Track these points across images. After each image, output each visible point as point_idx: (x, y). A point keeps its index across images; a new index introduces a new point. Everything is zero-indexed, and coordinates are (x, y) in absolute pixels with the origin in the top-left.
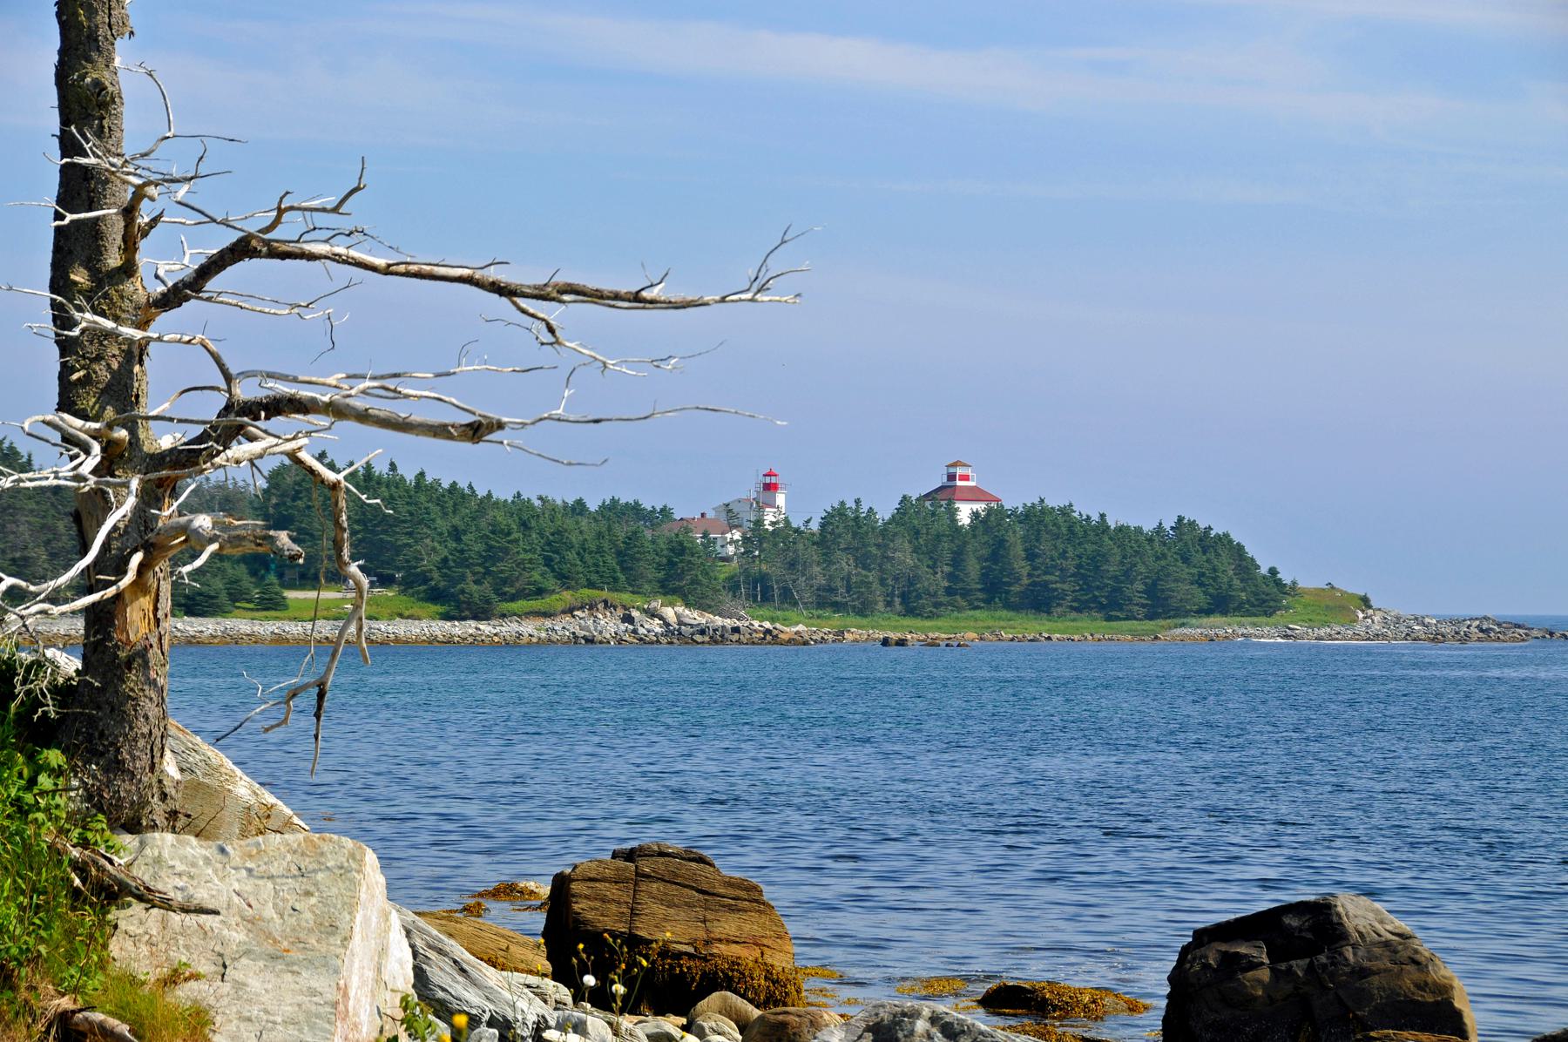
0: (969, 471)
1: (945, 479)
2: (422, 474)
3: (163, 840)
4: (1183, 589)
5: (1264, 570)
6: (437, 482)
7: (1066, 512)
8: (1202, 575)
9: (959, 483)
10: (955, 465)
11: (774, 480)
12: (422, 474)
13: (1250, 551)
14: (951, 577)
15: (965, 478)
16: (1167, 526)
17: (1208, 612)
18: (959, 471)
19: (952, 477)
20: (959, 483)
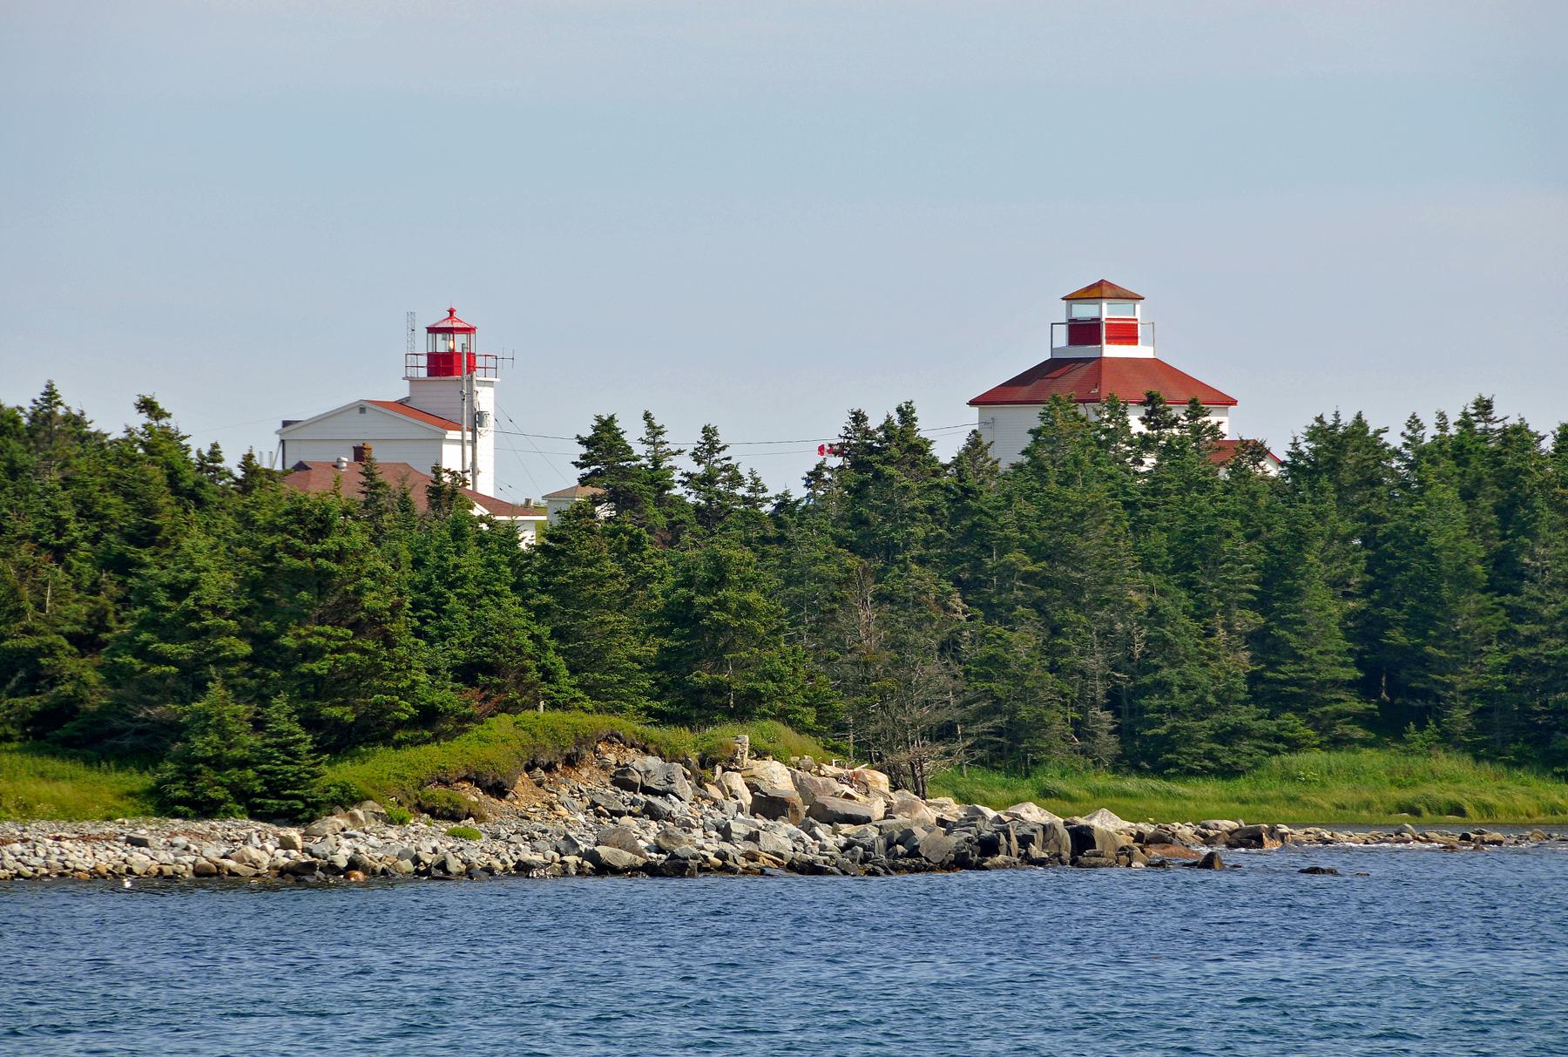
0: (1138, 312)
2: (1484, 407)
9: (1111, 351)
10: (1096, 292)
11: (457, 343)
12: (1484, 407)
14: (1259, 641)
15: (1126, 333)
19: (1083, 332)
20: (1111, 351)
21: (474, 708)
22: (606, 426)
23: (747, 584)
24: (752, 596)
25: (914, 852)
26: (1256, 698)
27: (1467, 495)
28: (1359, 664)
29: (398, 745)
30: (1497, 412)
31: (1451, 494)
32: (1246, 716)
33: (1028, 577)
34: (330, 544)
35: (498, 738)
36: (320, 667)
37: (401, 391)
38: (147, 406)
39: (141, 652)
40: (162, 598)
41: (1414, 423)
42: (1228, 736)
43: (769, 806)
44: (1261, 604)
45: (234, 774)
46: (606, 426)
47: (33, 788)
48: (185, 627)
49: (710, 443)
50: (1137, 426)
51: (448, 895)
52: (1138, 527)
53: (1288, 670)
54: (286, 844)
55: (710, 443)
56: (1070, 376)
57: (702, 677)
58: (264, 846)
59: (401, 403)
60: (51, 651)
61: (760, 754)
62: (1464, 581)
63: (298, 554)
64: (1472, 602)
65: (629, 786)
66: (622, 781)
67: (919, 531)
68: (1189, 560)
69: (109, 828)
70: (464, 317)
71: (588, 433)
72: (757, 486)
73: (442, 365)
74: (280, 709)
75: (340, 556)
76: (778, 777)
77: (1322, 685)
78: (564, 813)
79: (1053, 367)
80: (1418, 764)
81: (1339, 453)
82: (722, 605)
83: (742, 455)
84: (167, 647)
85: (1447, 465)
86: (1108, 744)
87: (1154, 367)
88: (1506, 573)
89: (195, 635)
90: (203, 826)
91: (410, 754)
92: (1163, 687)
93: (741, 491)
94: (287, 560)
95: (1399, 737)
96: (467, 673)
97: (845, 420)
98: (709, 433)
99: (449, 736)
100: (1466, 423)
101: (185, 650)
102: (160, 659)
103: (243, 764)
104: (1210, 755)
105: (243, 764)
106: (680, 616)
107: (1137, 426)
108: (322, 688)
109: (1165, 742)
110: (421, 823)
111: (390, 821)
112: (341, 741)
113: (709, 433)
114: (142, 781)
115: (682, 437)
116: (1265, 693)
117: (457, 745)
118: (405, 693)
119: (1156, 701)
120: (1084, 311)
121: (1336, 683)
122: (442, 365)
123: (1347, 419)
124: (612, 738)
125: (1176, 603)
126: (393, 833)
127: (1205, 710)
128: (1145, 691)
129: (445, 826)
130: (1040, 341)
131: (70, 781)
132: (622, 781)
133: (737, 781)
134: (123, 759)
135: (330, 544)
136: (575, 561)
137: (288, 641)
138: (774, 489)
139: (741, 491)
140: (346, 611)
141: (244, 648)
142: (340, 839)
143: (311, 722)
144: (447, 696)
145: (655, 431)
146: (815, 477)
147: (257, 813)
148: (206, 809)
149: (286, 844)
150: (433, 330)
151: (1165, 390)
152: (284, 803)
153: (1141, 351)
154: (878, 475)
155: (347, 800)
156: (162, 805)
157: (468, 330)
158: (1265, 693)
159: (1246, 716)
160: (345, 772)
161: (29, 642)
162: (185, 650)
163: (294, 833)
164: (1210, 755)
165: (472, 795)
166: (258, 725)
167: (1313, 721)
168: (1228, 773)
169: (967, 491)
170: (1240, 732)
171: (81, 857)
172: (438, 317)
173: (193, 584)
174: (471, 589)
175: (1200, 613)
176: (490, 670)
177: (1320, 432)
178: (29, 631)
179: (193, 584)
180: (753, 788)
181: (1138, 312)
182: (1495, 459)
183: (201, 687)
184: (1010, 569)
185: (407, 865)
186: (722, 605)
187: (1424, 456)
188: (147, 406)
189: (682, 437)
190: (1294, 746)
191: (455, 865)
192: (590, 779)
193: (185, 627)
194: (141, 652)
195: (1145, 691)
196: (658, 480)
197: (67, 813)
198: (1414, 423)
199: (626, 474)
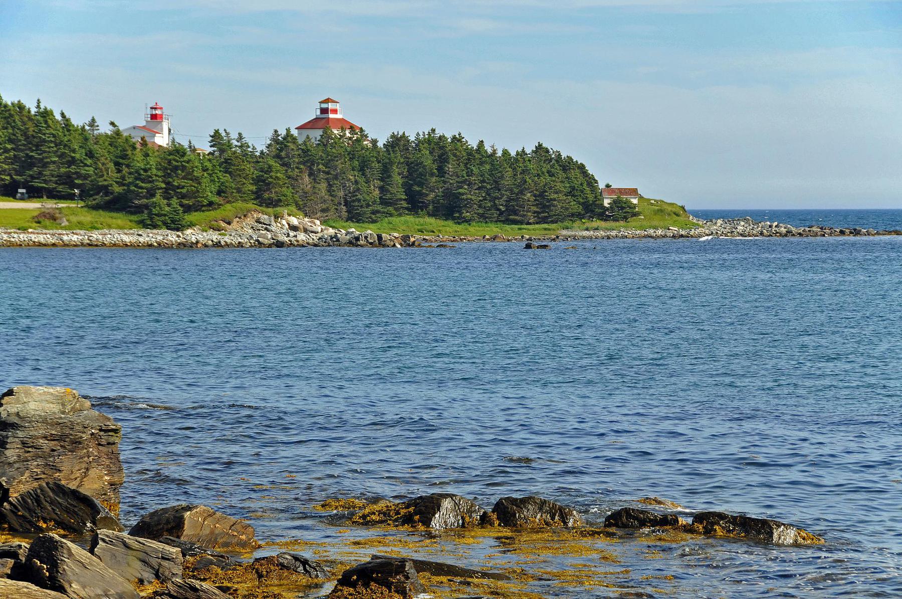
0: (337, 106)
1: (318, 112)
2: (433, 130)
3: (187, 535)
4: (561, 201)
5: (205, 147)
6: (505, 153)
7: (457, 139)
8: (573, 188)
9: (331, 116)
10: (327, 101)
11: (158, 112)
12: (433, 130)
13: (591, 170)
14: (382, 189)
15: (335, 111)
16: (528, 151)
17: (580, 216)
18: (331, 106)
19: (324, 111)
20: (331, 116)
21: (222, 202)
22: (217, 132)
23: (277, 171)
24: (279, 175)
25: (338, 240)
26: (381, 203)
27: (431, 153)
28: (406, 195)
29: (203, 211)
30: (437, 132)
31: (428, 152)
32: (379, 208)
33: (323, 172)
34: (185, 159)
35: (228, 209)
36: (184, 191)
37: (144, 124)
38: (112, 124)
39: (136, 186)
40: (142, 172)
41: (418, 134)
42: (374, 212)
43: (294, 228)
44: (382, 180)
45: (163, 218)
46: (217, 132)
47: (110, 221)
48: (148, 180)
49: (240, 137)
50: (348, 135)
51: (283, 252)
52: (351, 159)
53: (389, 196)
54: (178, 236)
55: (240, 137)
56: (322, 121)
57: (266, 196)
58: (172, 237)
59: (144, 127)
60: (111, 185)
61: (289, 215)
62: (432, 175)
63: (177, 161)
64: (434, 179)
65: (260, 223)
66: (258, 221)
67: (297, 160)
68: (363, 168)
69: (132, 231)
70: (160, 105)
71: (212, 134)
72: (254, 148)
73: (154, 117)
74: (175, 201)
75: (188, 162)
76: (294, 221)
77: (397, 200)
78: (241, 232)
79: (317, 119)
80: (421, 220)
81: (397, 142)
82: (271, 177)
83: (249, 139)
84: (143, 185)
85: (426, 145)
86: (345, 214)
87: (343, 121)
88: (441, 172)
89: (150, 182)
90: (155, 231)
91: (207, 213)
92: (359, 200)
93: (250, 149)
94: (174, 163)
95: (417, 213)
96: (219, 193)
97: (273, 132)
98: (240, 134)
99: (215, 209)
100: (429, 134)
101: (149, 185)
102: (142, 188)
103: (165, 215)
104: (370, 217)
105: (165, 215)
106: (258, 181)
107: (348, 135)
108: (184, 196)
109: (359, 215)
110: (211, 232)
111: (203, 231)
112: (188, 209)
113: (240, 134)
114: (135, 218)
115: (234, 135)
116: (384, 202)
117: (218, 211)
118: (206, 198)
119: (357, 204)
120: (324, 106)
121: (401, 199)
122: (154, 117)
123: (401, 133)
124: (255, 211)
125: (362, 180)
126: (205, 234)
127: (368, 205)
128: (354, 201)
129: (217, 232)
130: (313, 113)
131: (120, 218)
132: (258, 221)
133: (284, 222)
134: (132, 213)
135: (185, 159)
136: (234, 165)
137: (175, 184)
138: (259, 149)
139: (250, 149)
140: (189, 176)
141: (164, 186)
142: (191, 235)
143: (182, 205)
144: (216, 199)
145: (227, 134)
146: (269, 146)
147: (169, 228)
148: (155, 227)
149: (178, 236)
150: (152, 108)
151: (343, 124)
152: (176, 226)
153: (339, 116)
154: (286, 146)
155: (191, 225)
156: (143, 224)
157: (161, 108)
158: (384, 202)
159: (379, 208)
160: (194, 216)
161: (106, 183)
162: (149, 185)
163: (179, 233)
164: (370, 217)
165: (223, 224)
166: (169, 205)
167: (396, 209)
168: (374, 222)
169: (308, 150)
170: (378, 212)
171: (127, 239)
172: (153, 105)
173: (150, 169)
174: (210, 172)
175: (367, 182)
176: (224, 192)
177: (393, 136)
178: (105, 180)
179: (150, 169)
180: (289, 224)
181: (337, 106)
182: (437, 144)
183: (153, 195)
184: (319, 170)
185: (210, 242)
186: (271, 177)
187: (419, 142)
188: (112, 124)
189: (234, 135)
190: (391, 215)
191: (223, 243)
192: (250, 221)
193: (148, 180)
194: (136, 186)
195: (354, 201)
196: (230, 146)
197: (121, 228)
198: (418, 134)
199: (223, 145)
